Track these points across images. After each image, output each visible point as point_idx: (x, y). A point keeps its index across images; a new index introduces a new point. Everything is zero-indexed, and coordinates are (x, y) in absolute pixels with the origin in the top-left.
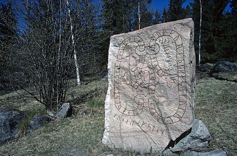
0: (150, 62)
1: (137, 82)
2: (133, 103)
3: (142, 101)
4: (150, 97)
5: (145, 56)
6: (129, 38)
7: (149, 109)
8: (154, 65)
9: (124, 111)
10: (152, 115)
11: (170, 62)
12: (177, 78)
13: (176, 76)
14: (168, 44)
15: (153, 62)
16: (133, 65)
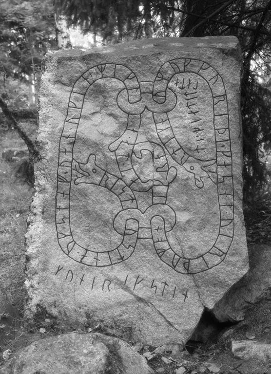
0: (155, 129)
1: (122, 176)
2: (109, 233)
3: (134, 226)
4: (155, 214)
5: (140, 114)
6: (99, 66)
7: (152, 242)
8: (164, 136)
9: (84, 256)
10: (160, 257)
11: (200, 132)
12: (214, 168)
13: (212, 162)
14: (195, 91)
15: (162, 130)
16: (111, 136)
